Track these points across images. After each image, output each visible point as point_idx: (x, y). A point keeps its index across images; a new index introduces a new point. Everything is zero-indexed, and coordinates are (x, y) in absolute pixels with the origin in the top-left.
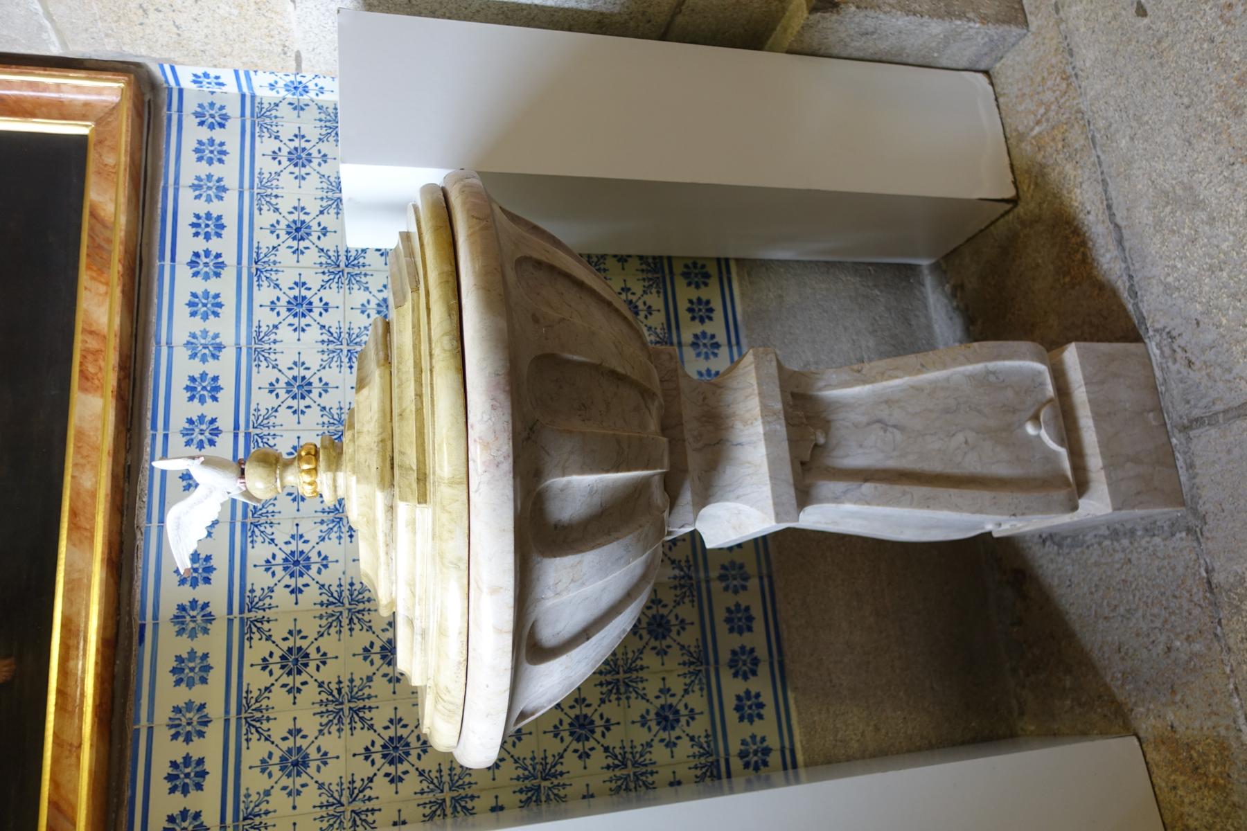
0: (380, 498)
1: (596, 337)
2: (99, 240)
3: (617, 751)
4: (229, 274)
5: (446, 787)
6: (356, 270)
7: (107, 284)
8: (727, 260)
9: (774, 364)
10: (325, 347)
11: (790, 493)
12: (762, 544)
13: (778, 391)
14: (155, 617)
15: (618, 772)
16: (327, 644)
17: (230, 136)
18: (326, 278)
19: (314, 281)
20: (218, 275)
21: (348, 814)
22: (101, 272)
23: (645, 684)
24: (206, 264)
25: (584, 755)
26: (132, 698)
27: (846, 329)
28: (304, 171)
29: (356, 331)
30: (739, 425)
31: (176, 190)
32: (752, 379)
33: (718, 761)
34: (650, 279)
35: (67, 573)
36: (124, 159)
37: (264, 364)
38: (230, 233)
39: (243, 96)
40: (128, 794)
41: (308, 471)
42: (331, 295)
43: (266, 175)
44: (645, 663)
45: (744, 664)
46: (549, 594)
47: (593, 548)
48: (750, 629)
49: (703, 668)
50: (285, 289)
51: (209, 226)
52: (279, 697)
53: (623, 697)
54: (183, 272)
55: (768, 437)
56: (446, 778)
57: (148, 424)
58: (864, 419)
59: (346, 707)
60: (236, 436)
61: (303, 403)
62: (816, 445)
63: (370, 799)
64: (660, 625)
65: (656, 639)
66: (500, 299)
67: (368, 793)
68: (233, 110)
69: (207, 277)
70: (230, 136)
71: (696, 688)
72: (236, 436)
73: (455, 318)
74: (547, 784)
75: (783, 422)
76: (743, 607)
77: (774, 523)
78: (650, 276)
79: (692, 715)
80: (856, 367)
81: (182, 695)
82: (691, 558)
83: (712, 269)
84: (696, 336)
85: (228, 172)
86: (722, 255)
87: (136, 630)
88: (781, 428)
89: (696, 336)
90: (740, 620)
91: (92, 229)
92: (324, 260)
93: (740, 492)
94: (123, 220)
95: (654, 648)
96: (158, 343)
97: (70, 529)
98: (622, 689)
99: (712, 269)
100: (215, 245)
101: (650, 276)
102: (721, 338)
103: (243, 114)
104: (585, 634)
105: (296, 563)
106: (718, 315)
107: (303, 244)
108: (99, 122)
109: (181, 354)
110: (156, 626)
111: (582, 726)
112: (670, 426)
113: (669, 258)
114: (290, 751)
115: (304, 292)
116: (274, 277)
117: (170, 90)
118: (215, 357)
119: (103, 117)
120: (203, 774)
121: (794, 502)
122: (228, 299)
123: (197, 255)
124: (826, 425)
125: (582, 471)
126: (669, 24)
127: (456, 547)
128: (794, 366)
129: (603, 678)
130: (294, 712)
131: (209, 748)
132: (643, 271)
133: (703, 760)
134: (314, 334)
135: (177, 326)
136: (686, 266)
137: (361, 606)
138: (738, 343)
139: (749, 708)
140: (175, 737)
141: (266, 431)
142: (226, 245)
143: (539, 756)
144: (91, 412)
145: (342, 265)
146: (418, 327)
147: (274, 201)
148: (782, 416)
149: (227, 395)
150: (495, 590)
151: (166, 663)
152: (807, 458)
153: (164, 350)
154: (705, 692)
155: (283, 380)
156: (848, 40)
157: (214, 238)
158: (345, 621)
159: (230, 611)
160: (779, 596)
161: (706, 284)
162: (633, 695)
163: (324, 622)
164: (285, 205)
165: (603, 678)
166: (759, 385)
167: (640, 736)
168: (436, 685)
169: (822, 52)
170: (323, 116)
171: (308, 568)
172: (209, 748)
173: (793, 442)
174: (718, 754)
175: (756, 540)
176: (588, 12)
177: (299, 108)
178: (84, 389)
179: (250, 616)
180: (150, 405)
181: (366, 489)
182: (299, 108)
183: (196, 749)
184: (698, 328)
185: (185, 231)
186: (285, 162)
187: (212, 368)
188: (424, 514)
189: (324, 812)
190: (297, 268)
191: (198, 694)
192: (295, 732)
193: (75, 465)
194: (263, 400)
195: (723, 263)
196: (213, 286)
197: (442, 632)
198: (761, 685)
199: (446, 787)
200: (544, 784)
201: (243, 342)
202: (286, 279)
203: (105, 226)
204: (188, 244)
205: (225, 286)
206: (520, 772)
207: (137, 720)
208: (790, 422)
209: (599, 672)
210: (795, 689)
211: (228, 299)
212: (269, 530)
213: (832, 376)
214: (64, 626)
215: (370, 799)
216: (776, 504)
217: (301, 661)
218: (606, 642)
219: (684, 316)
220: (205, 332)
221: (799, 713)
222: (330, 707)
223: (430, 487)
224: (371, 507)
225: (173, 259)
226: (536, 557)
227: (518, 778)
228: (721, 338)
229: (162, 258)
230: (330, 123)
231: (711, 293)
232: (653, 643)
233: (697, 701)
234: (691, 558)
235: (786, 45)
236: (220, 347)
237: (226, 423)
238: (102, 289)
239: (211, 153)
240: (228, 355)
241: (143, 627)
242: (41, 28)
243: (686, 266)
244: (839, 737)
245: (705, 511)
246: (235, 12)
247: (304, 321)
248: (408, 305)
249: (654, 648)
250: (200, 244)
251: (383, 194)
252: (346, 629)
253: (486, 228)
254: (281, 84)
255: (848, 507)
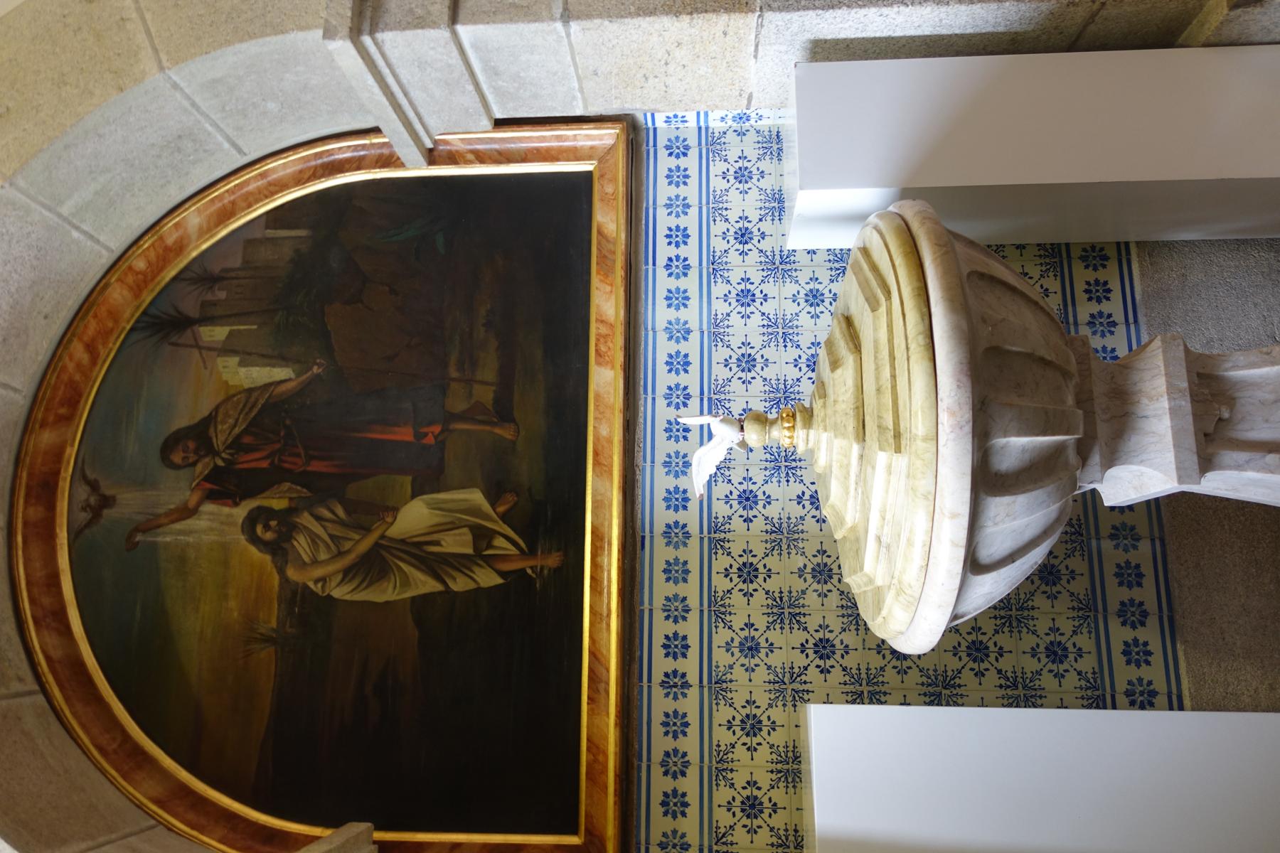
0: (856, 448)
1: (1026, 331)
2: (604, 252)
3: (1009, 674)
4: (694, 273)
5: (864, 683)
6: (788, 267)
7: (612, 285)
8: (1127, 244)
9: (1182, 348)
10: (765, 330)
11: (1192, 460)
12: (1155, 507)
13: (1184, 371)
14: (651, 532)
15: (1009, 692)
16: (772, 562)
17: (691, 163)
18: (765, 274)
19: (756, 276)
20: (685, 275)
21: (789, 691)
22: (606, 276)
23: (1035, 622)
24: (677, 267)
25: (979, 674)
26: (637, 587)
27: (1255, 305)
28: (747, 186)
29: (789, 317)
30: (1145, 401)
31: (655, 209)
32: (1159, 361)
33: (1104, 695)
34: (1047, 264)
35: (593, 496)
36: (621, 189)
37: (720, 344)
38: (694, 241)
39: (700, 128)
40: (638, 654)
41: (788, 428)
42: (769, 288)
43: (719, 192)
44: (1036, 604)
45: (1133, 614)
46: (990, 523)
47: (1024, 492)
48: (1140, 585)
49: (1092, 614)
50: (735, 284)
51: (678, 236)
52: (737, 599)
53: (1015, 630)
54: (662, 273)
55: (1173, 412)
56: (864, 676)
57: (642, 389)
58: (1271, 397)
59: (786, 611)
60: (702, 400)
61: (750, 375)
62: (1220, 419)
63: (805, 682)
64: (1050, 573)
65: (1047, 585)
66: (960, 303)
67: (803, 677)
68: (692, 141)
69: (678, 277)
70: (691, 163)
71: (1085, 630)
72: (702, 400)
73: (927, 321)
74: (948, 692)
75: (1188, 398)
76: (1133, 564)
77: (1176, 484)
78: (1048, 260)
79: (1080, 653)
80: (1265, 350)
81: (671, 589)
82: (1082, 517)
83: (1112, 252)
84: (1092, 316)
85: (690, 192)
86: (1122, 239)
87: (639, 539)
88: (1186, 404)
89: (1092, 316)
90: (1130, 575)
91: (599, 243)
92: (763, 259)
93: (1144, 457)
94: (623, 236)
95: (1044, 592)
96: (646, 329)
97: (594, 465)
98: (1015, 624)
99: (1112, 252)
100: (683, 251)
101: (1048, 260)
102: (1119, 317)
103: (700, 144)
104: (1011, 558)
105: (747, 499)
106: (1116, 295)
107: (747, 247)
108: (600, 161)
109: (662, 337)
110: (652, 537)
111: (978, 650)
112: (1084, 400)
113: (1067, 245)
114: (746, 638)
115: (749, 286)
116: (726, 275)
117: (648, 129)
118: (685, 339)
119: (603, 156)
120: (687, 647)
121: (1196, 467)
122: (693, 293)
123: (670, 259)
124: (1231, 402)
125: (1019, 434)
126: (1079, 35)
127: (925, 484)
128: (1197, 347)
129: (997, 613)
130: (748, 610)
131: (690, 628)
132: (1040, 256)
133: (1089, 693)
134: (757, 319)
135: (659, 315)
136: (1085, 250)
137: (796, 536)
138: (1136, 321)
139: (1136, 654)
140: (667, 618)
141: (723, 397)
142: (690, 251)
143: (941, 669)
144: (604, 380)
145: (777, 263)
146: (891, 326)
147: (724, 213)
148: (1187, 394)
149: (694, 368)
150: (954, 516)
151: (659, 565)
152: (1210, 430)
153: (651, 333)
154: (1093, 635)
155: (735, 357)
156: (1272, 27)
157: (682, 246)
158: (784, 547)
159: (701, 532)
160: (1171, 558)
161: (1104, 266)
162: (1025, 630)
163: (768, 546)
164: (733, 216)
165: (997, 613)
166: (1166, 366)
167: (1031, 665)
168: (900, 582)
169: (1243, 39)
170: (760, 139)
171: (756, 503)
172: (690, 628)
173: (1197, 417)
174: (1104, 690)
175: (1148, 502)
176: (1003, 33)
177: (741, 134)
178: (598, 363)
179: (716, 536)
180: (642, 376)
181: (839, 443)
182: (741, 134)
183: (682, 628)
184: (1094, 308)
185: (662, 241)
186: (732, 180)
187: (684, 347)
188: (901, 461)
189: (771, 687)
190: (745, 266)
191: (681, 589)
192: (749, 625)
193: (596, 418)
194: (721, 373)
195: (1123, 248)
196: (683, 283)
197: (910, 543)
198: (1150, 634)
199: (864, 683)
200: (944, 692)
201: (705, 327)
202: (735, 276)
203: (608, 241)
204: (664, 251)
205: (690, 283)
206: (924, 679)
207: (642, 603)
208: (1195, 399)
209: (994, 607)
210: (1185, 642)
211: (693, 293)
212: (727, 473)
213: (1240, 358)
214: (593, 532)
215: (805, 682)
216: (1178, 469)
217: (753, 573)
218: (1026, 567)
219: (1081, 296)
220: (678, 320)
221: (1188, 664)
222: (775, 610)
223: (903, 443)
224: (847, 455)
225: (654, 264)
226: (983, 496)
227: (923, 684)
228: (1119, 317)
229: (647, 263)
230: (773, 144)
231: (1110, 274)
232: (1043, 588)
233: (1085, 641)
234: (1082, 517)
235: (1203, 39)
236: (688, 332)
237: (694, 390)
238: (608, 288)
239: (678, 177)
240: (695, 337)
241: (643, 537)
242: (574, 98)
243: (1085, 250)
244: (1230, 689)
245: (1112, 472)
246: (710, 71)
247: (749, 310)
248: (883, 309)
249: (1044, 592)
250: (672, 251)
251: (836, 210)
252: (785, 553)
253: (946, 253)
254: (730, 116)
255: (1251, 474)
